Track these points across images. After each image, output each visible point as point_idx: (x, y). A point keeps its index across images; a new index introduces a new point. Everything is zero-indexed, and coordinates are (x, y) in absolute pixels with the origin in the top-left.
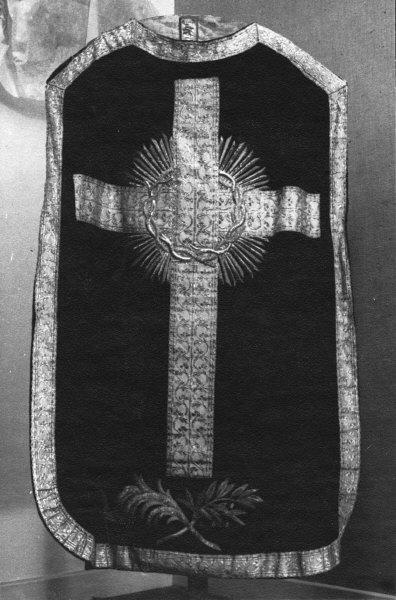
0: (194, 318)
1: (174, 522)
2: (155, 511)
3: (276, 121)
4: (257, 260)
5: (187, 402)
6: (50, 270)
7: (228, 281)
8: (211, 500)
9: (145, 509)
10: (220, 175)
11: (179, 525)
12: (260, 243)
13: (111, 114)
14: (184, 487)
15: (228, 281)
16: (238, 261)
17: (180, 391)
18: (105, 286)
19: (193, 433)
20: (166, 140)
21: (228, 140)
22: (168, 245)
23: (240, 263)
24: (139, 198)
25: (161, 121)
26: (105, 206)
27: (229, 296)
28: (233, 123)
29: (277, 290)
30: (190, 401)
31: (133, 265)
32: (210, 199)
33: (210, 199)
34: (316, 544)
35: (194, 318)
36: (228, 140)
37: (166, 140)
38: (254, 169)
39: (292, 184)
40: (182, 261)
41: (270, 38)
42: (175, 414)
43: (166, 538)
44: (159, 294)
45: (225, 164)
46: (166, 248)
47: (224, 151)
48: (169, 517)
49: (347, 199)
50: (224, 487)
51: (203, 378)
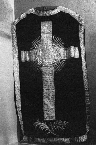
0: (49, 78)
2: (42, 128)
3: (67, 29)
9: (40, 126)
10: (53, 45)
11: (48, 131)
13: (26, 34)
18: (29, 75)
22: (41, 62)
25: (37, 34)
26: (25, 56)
28: (55, 33)
29: (68, 71)
31: (37, 71)
32: (50, 53)
33: (50, 53)
34: (82, 134)
35: (49, 78)
39: (72, 46)
40: (44, 67)
44: (40, 74)
49: (85, 55)
50: (60, 121)
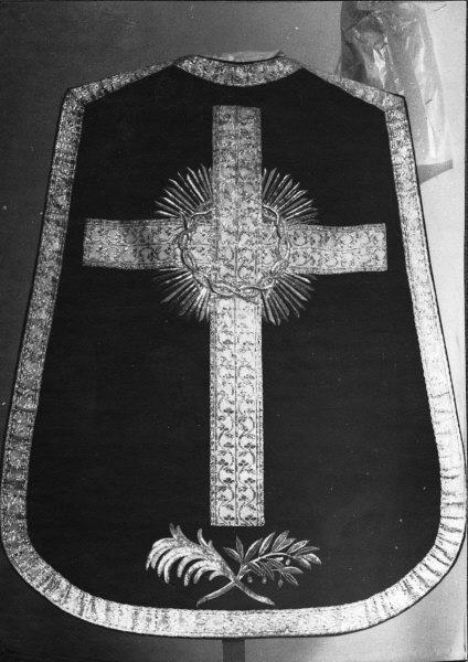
1: (216, 578)
4: (303, 298)
5: (233, 450)
6: (416, 318)
7: (273, 321)
8: (266, 553)
11: (222, 580)
12: (307, 280)
14: (223, 539)
15: (273, 321)
16: (281, 297)
17: (224, 437)
19: (240, 485)
20: (205, 170)
21: (273, 172)
23: (284, 300)
24: (165, 233)
27: (275, 340)
28: (277, 157)
30: (236, 450)
36: (273, 172)
37: (205, 170)
38: (301, 201)
41: (82, 94)
42: (220, 463)
43: (204, 600)
44: (195, 335)
45: (268, 197)
46: (205, 284)
47: (269, 184)
48: (212, 571)
51: (248, 424)
